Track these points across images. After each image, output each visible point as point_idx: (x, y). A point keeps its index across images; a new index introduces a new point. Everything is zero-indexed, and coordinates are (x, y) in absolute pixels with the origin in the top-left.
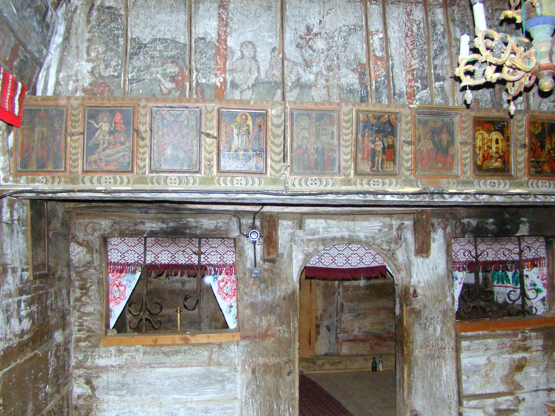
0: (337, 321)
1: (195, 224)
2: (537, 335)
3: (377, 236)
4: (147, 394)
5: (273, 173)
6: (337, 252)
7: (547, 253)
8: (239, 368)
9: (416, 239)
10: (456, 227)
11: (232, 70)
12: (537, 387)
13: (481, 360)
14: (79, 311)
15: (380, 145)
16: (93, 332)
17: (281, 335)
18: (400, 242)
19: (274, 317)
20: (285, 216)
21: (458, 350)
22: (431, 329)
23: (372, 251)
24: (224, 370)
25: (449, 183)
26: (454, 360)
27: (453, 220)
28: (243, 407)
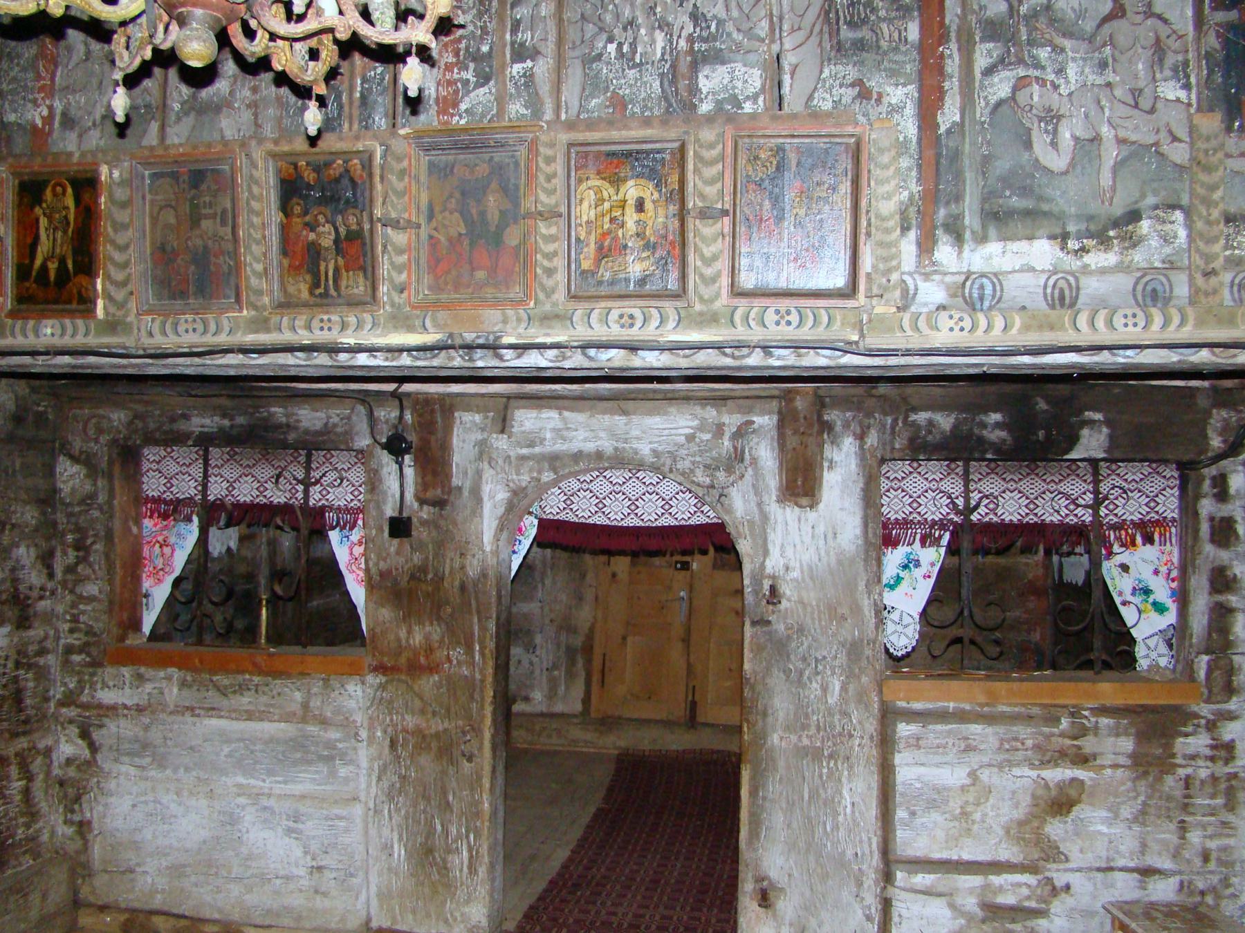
1: (284, 420)
2: (1117, 726)
3: (683, 452)
4: (187, 769)
5: (112, 310)
6: (609, 488)
8: (364, 734)
11: (66, 89)
12: (1109, 859)
14: (72, 592)
15: (329, 233)
16: (95, 634)
20: (465, 402)
21: (886, 743)
22: (814, 685)
24: (334, 734)
25: (505, 321)
26: (874, 769)
27: (886, 414)
28: (370, 819)
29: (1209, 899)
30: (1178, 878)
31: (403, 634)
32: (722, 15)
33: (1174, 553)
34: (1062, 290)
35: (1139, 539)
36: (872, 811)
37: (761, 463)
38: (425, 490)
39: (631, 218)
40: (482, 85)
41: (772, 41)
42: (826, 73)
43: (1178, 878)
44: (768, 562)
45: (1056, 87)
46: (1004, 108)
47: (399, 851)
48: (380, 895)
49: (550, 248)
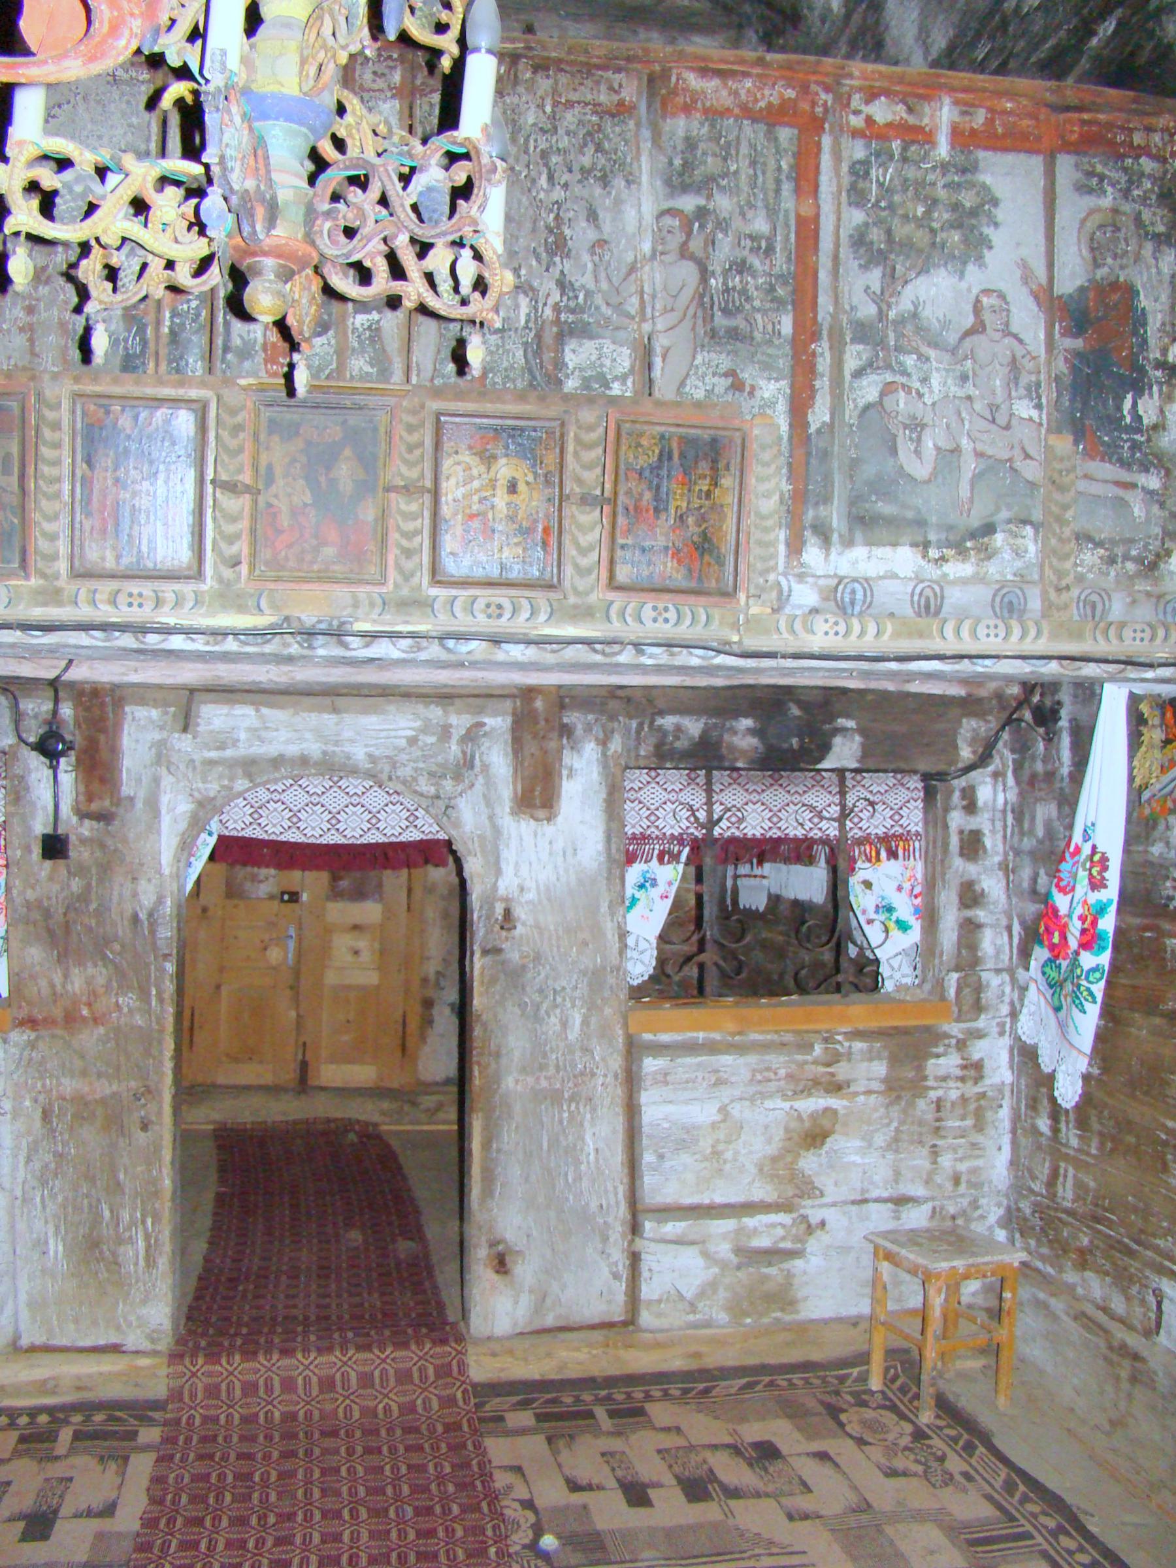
2: (870, 1050)
3: (404, 757)
6: (306, 799)
7: (926, 822)
10: (638, 738)
12: (863, 1191)
13: (703, 1113)
18: (468, 775)
21: (631, 1081)
22: (553, 1019)
28: (17, 1211)
29: (960, 1222)
30: (930, 1205)
31: (58, 979)
32: (591, 286)
33: (918, 867)
34: (928, 600)
35: (883, 854)
36: (617, 1158)
37: (493, 770)
38: (90, 799)
39: (501, 500)
40: (319, 335)
41: (643, 319)
42: (699, 359)
43: (930, 1205)
44: (500, 883)
45: (920, 395)
46: (872, 413)
47: (56, 1247)
48: (29, 1304)
49: (410, 526)
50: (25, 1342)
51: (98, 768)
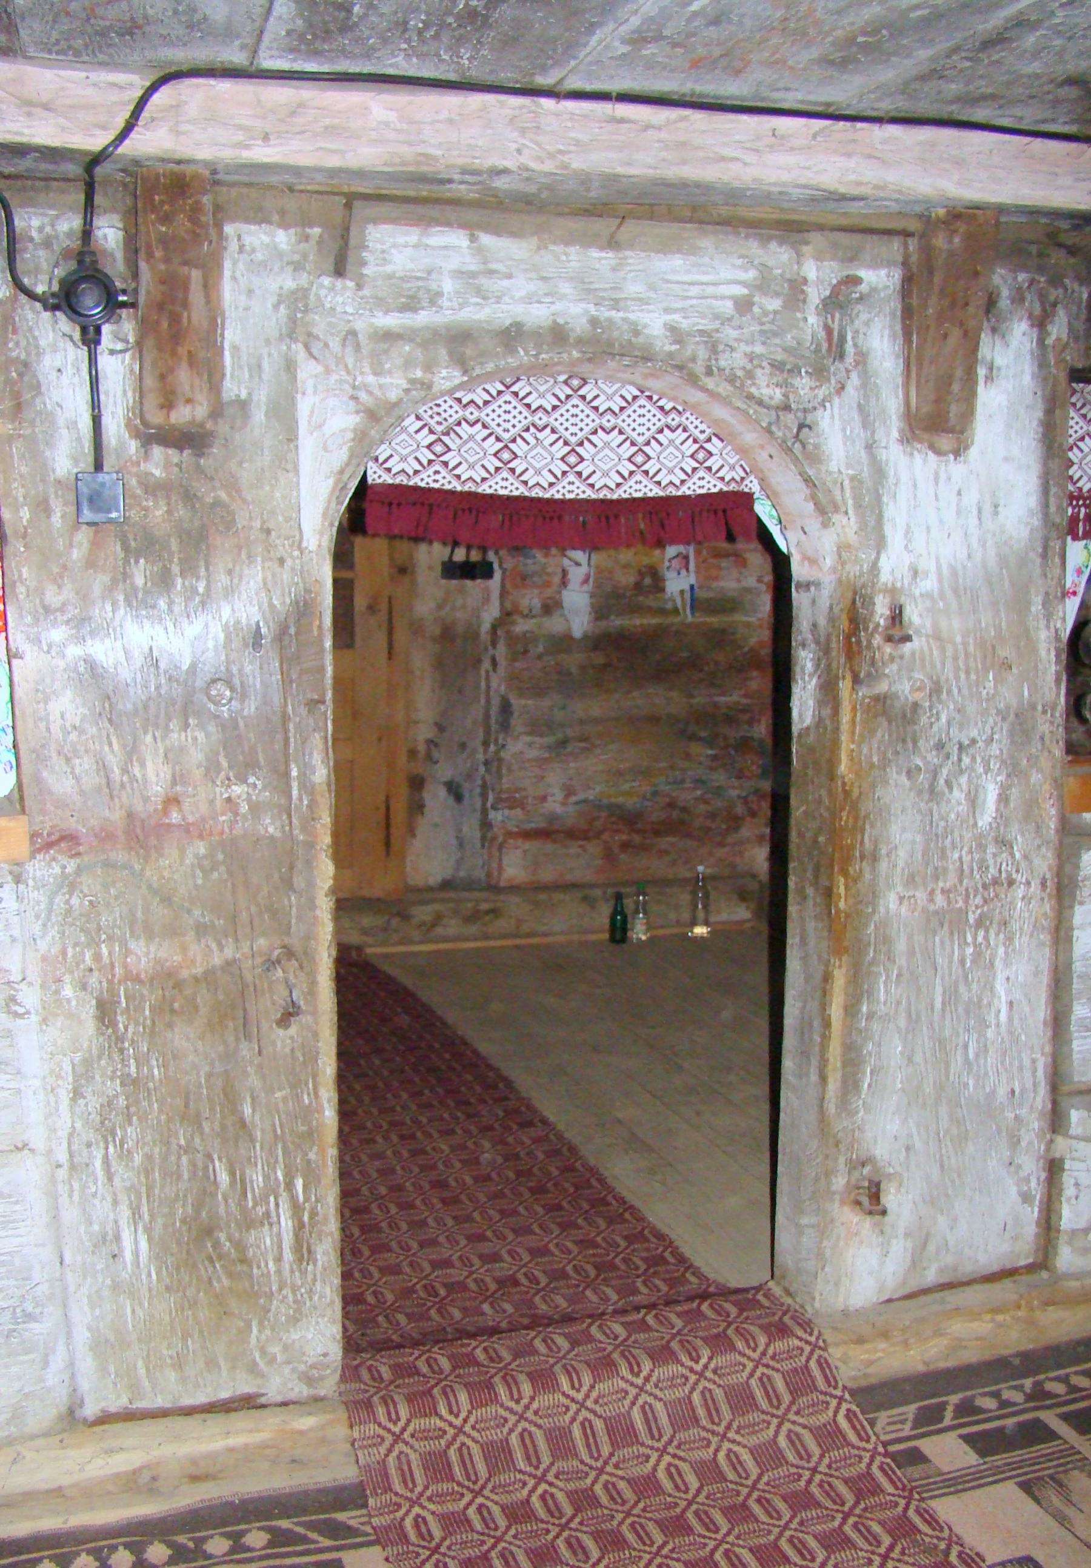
0: (486, 763)
3: (730, 333)
6: (524, 418)
8: (30, 997)
9: (912, 364)
17: (238, 829)
18: (836, 369)
19: (201, 736)
23: (690, 420)
26: (1045, 937)
47: (135, 1244)
50: (91, 1410)
51: (177, 337)
